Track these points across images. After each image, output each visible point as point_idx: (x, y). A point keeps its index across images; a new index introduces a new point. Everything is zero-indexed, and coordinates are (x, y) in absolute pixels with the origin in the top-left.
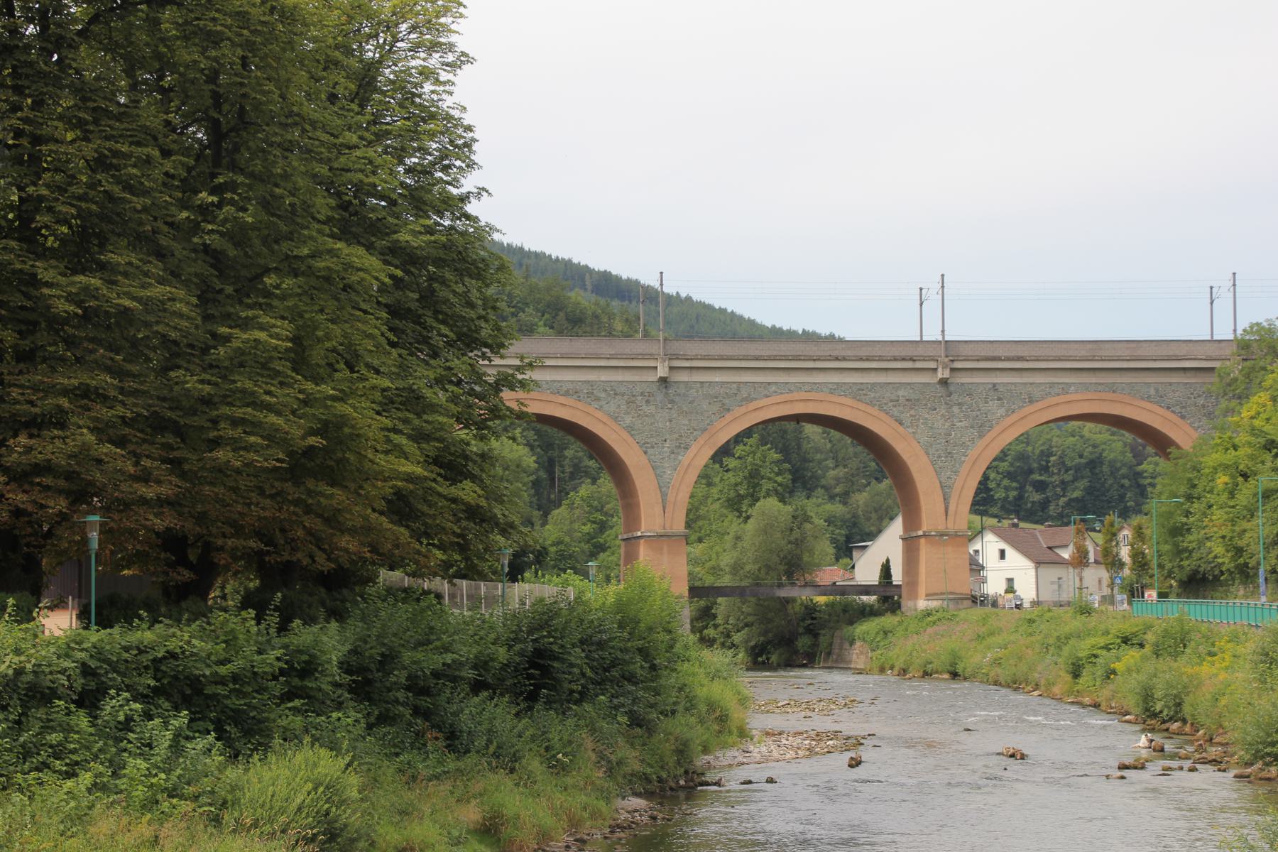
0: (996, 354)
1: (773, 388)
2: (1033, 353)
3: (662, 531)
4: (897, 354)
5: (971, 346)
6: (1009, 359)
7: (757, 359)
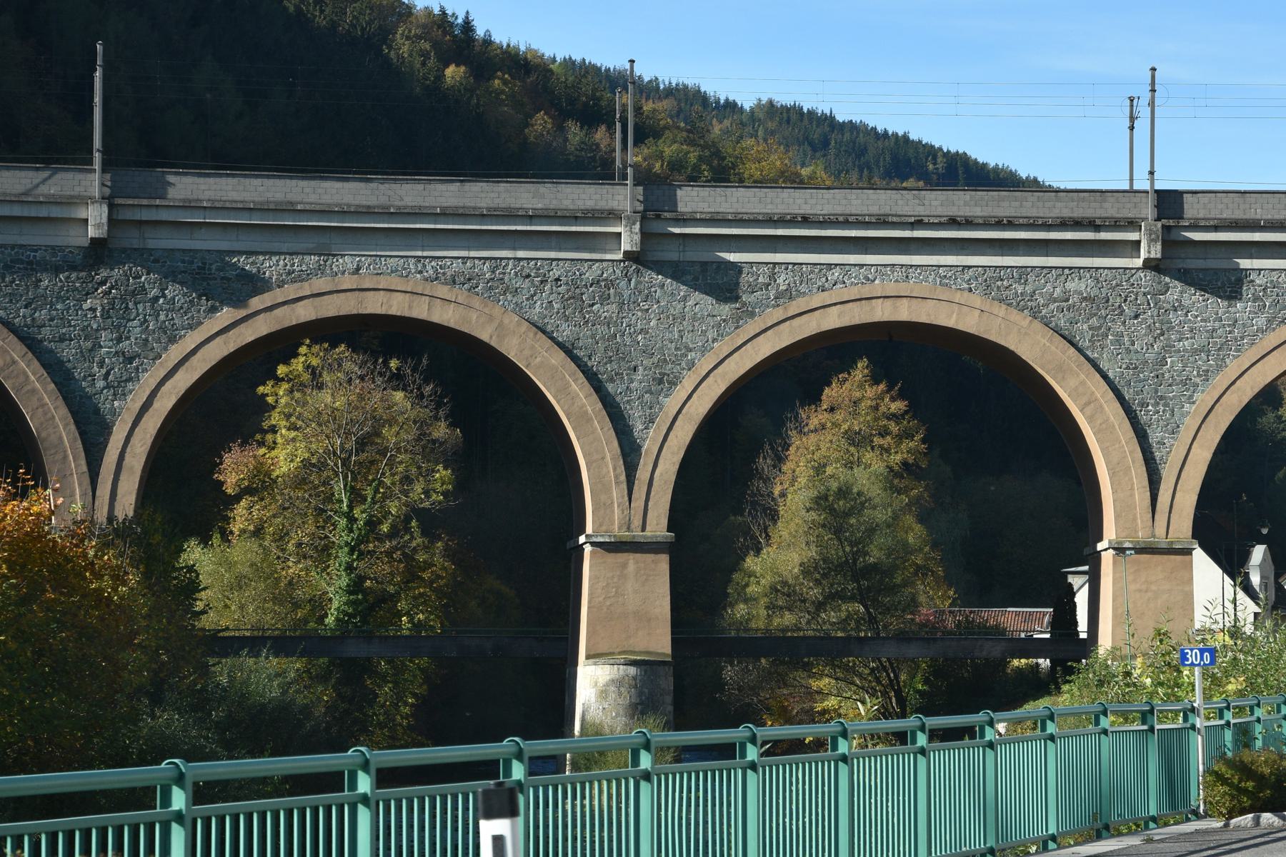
0: (1250, 215)
1: (837, 273)
3: (625, 535)
4: (1066, 213)
6: (986, 225)
7: (806, 221)
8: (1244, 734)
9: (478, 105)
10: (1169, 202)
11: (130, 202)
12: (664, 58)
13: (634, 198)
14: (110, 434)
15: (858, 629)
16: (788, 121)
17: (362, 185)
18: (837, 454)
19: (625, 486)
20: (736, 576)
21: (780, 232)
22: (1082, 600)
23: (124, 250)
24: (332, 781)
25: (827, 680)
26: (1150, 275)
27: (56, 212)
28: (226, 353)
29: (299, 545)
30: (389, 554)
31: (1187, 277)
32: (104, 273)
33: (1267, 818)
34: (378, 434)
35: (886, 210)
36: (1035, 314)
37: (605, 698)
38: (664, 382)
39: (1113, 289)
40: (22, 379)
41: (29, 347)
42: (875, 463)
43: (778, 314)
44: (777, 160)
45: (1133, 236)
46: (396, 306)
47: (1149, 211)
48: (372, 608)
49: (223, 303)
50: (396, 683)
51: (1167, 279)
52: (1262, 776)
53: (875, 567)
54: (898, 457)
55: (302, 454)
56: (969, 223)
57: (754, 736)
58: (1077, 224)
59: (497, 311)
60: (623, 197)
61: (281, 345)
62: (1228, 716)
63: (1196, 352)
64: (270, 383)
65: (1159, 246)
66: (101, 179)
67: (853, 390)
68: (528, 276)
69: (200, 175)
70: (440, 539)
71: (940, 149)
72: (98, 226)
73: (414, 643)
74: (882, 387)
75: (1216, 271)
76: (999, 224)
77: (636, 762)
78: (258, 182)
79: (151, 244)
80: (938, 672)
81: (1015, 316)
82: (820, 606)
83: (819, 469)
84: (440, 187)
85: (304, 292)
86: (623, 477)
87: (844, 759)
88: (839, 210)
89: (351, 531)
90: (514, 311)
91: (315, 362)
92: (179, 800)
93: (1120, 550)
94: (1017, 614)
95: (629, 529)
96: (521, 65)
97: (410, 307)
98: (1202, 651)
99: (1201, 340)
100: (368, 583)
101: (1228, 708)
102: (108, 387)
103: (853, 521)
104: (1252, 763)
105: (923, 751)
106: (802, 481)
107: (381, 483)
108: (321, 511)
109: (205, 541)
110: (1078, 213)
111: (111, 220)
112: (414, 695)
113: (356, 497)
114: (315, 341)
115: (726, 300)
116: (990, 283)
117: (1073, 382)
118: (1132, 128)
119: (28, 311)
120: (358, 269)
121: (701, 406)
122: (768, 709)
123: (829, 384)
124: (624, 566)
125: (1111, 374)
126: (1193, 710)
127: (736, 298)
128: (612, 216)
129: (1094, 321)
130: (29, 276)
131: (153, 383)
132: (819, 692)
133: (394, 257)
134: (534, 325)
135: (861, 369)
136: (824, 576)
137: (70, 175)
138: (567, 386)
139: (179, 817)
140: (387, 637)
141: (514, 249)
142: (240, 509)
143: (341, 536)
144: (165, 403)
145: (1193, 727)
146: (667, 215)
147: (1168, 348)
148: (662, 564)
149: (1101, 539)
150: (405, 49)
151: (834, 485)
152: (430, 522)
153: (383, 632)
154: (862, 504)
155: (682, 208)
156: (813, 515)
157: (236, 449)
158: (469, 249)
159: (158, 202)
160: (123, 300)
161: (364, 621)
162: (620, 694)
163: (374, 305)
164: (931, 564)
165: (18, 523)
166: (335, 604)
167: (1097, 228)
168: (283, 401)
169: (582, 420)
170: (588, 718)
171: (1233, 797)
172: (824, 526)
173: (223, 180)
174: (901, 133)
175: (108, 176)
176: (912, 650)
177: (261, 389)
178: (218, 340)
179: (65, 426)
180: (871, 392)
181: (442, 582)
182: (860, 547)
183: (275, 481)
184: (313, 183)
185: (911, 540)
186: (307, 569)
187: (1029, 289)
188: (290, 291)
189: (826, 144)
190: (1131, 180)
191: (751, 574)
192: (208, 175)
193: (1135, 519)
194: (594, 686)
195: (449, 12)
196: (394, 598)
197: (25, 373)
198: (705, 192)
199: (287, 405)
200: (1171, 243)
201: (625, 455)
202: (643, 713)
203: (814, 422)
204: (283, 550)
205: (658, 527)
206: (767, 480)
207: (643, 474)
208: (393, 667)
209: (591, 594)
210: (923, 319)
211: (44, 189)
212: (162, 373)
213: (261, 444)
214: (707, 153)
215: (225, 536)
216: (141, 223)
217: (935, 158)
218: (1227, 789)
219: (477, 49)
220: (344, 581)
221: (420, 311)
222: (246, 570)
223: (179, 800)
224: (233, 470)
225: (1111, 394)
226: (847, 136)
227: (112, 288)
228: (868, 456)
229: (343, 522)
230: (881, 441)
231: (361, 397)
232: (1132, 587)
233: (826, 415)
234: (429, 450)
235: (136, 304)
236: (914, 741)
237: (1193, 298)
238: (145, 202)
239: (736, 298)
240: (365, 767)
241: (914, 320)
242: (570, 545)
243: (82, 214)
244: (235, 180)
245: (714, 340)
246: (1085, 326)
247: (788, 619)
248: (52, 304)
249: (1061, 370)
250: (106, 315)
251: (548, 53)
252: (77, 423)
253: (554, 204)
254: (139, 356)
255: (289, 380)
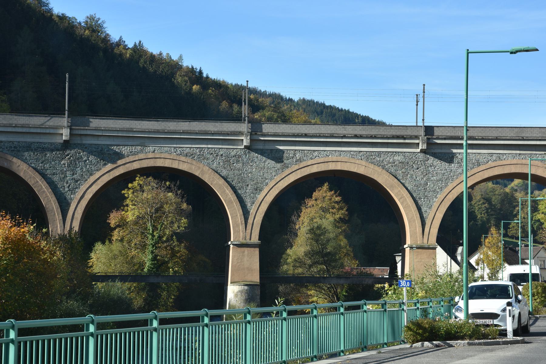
1: (316, 153)
2: (480, 134)
3: (244, 241)
4: (394, 133)
5: (441, 129)
6: (367, 137)
7: (306, 136)
8: (425, 312)
9: (203, 98)
10: (429, 130)
11: (77, 128)
12: (265, 83)
13: (248, 127)
14: (70, 206)
15: (324, 274)
16: (310, 105)
17: (156, 122)
18: (318, 214)
19: (244, 225)
20: (284, 256)
21: (297, 139)
22: (399, 265)
23: (75, 144)
24: (145, 323)
25: (313, 291)
26: (422, 154)
27: (52, 131)
28: (109, 179)
29: (136, 244)
30: (166, 247)
31: (435, 155)
32: (68, 152)
33: (427, 344)
34: (163, 207)
35: (333, 132)
36: (383, 167)
37: (237, 297)
38: (258, 190)
39: (410, 159)
40: (40, 187)
41: (43, 177)
42: (330, 218)
43: (297, 167)
44: (303, 118)
45: (417, 141)
46: (167, 164)
47: (422, 133)
48: (160, 266)
49: (108, 162)
50: (168, 291)
51: (428, 156)
52: (425, 328)
53: (329, 253)
54: (338, 216)
55: (137, 213)
56: (361, 137)
57: (285, 309)
58: (398, 137)
59: (201, 165)
60: (244, 127)
61: (129, 177)
62: (418, 305)
63: (438, 181)
64: (126, 190)
65: (426, 145)
66: (67, 119)
67: (323, 194)
68: (212, 154)
69: (101, 119)
70: (183, 243)
71: (360, 115)
72: (66, 136)
73: (173, 278)
74: (333, 192)
75: (445, 153)
76: (371, 137)
77: (245, 318)
78: (120, 121)
79: (84, 142)
80: (351, 288)
81: (376, 168)
82: (310, 266)
83: (312, 220)
84: (183, 123)
85: (135, 159)
86: (243, 222)
87: (316, 317)
88: (317, 132)
89: (153, 240)
90: (207, 165)
91: (141, 183)
92: (92, 329)
93: (411, 248)
94: (379, 269)
95: (245, 239)
96: (219, 85)
97: (172, 164)
98: (406, 281)
99: (440, 177)
100: (159, 257)
101: (418, 302)
102: (69, 190)
103: (322, 237)
104: (422, 323)
105: (342, 314)
106: (306, 224)
107: (163, 224)
108: (143, 233)
109: (103, 243)
110: (399, 133)
111: (70, 134)
112: (174, 295)
113: (155, 228)
114: (142, 175)
115: (279, 162)
116: (368, 157)
117: (396, 191)
118: (417, 105)
119: (42, 165)
120: (154, 151)
121: (270, 198)
122: (294, 301)
123: (315, 191)
124: (244, 252)
125: (409, 188)
126: (403, 303)
127: (283, 162)
128: (241, 133)
129: (403, 170)
130: (43, 153)
131: (85, 189)
132: (311, 295)
133: (167, 147)
134: (214, 170)
135: (326, 186)
136: (312, 256)
137: (57, 119)
138: (225, 191)
139: (92, 335)
140: (164, 276)
141: (207, 144)
142: (116, 232)
143: (149, 242)
144: (89, 196)
145: (403, 310)
146: (259, 133)
147: (428, 179)
148: (257, 251)
149: (405, 244)
150: (179, 80)
151: (316, 225)
152: (180, 237)
153: (164, 274)
154: (325, 232)
155: (264, 131)
156: (309, 235)
157: (114, 211)
158: (192, 144)
159: (87, 128)
160: (75, 161)
161: (157, 270)
162: (242, 295)
163: (160, 163)
164: (349, 253)
165: (16, 235)
166: (147, 265)
167: (405, 139)
168: (130, 196)
169: (230, 202)
170: (231, 303)
171: (414, 336)
172: (312, 239)
173: (109, 121)
174: (347, 109)
175: (70, 119)
176: (342, 281)
177: (123, 192)
178: (106, 175)
179: (55, 204)
180: (329, 194)
181: (183, 257)
182: (324, 246)
183: (127, 223)
184: (139, 122)
185: (342, 244)
186: (138, 253)
187: (381, 159)
188: (131, 158)
189: (322, 113)
190: (417, 122)
191: (289, 255)
192: (104, 119)
193: (417, 237)
194: (233, 292)
195: (195, 67)
196: (167, 262)
197: (41, 186)
198: (272, 126)
199: (132, 197)
200: (430, 144)
201: (244, 214)
202: (249, 302)
203: (310, 204)
204: (130, 246)
205: (255, 239)
206: (295, 224)
207: (250, 221)
208: (167, 286)
209: (232, 262)
210: (346, 169)
211: (48, 123)
212: (88, 186)
213: (123, 210)
214: (280, 115)
215: (110, 241)
216: (81, 135)
217: (358, 118)
218: (412, 333)
219: (204, 80)
220: (150, 257)
221: (175, 165)
222: (116, 252)
223: (92, 329)
224: (113, 219)
225: (409, 195)
226: (329, 110)
227: (71, 157)
228: (328, 216)
229: (150, 237)
230: (332, 211)
231: (157, 194)
232: (416, 260)
233: (314, 201)
234: (180, 212)
235: (79, 162)
236: (339, 310)
237: (437, 162)
238: (82, 128)
239: (283, 162)
240: (92, 322)
241: (343, 169)
242: (226, 245)
243: (61, 132)
244: (113, 121)
245: (275, 176)
246: (400, 172)
247: (300, 270)
248: (50, 162)
249: (392, 187)
250: (69, 166)
251: (230, 82)
252: (59, 203)
253: (221, 129)
254: (80, 180)
255: (133, 189)
